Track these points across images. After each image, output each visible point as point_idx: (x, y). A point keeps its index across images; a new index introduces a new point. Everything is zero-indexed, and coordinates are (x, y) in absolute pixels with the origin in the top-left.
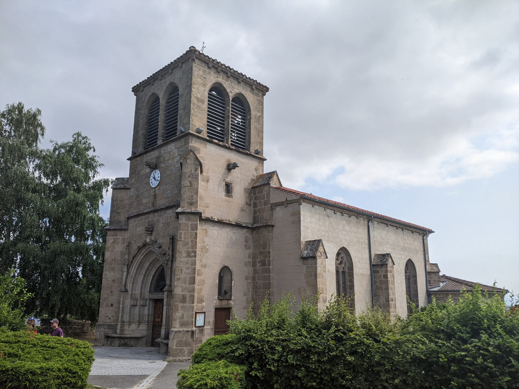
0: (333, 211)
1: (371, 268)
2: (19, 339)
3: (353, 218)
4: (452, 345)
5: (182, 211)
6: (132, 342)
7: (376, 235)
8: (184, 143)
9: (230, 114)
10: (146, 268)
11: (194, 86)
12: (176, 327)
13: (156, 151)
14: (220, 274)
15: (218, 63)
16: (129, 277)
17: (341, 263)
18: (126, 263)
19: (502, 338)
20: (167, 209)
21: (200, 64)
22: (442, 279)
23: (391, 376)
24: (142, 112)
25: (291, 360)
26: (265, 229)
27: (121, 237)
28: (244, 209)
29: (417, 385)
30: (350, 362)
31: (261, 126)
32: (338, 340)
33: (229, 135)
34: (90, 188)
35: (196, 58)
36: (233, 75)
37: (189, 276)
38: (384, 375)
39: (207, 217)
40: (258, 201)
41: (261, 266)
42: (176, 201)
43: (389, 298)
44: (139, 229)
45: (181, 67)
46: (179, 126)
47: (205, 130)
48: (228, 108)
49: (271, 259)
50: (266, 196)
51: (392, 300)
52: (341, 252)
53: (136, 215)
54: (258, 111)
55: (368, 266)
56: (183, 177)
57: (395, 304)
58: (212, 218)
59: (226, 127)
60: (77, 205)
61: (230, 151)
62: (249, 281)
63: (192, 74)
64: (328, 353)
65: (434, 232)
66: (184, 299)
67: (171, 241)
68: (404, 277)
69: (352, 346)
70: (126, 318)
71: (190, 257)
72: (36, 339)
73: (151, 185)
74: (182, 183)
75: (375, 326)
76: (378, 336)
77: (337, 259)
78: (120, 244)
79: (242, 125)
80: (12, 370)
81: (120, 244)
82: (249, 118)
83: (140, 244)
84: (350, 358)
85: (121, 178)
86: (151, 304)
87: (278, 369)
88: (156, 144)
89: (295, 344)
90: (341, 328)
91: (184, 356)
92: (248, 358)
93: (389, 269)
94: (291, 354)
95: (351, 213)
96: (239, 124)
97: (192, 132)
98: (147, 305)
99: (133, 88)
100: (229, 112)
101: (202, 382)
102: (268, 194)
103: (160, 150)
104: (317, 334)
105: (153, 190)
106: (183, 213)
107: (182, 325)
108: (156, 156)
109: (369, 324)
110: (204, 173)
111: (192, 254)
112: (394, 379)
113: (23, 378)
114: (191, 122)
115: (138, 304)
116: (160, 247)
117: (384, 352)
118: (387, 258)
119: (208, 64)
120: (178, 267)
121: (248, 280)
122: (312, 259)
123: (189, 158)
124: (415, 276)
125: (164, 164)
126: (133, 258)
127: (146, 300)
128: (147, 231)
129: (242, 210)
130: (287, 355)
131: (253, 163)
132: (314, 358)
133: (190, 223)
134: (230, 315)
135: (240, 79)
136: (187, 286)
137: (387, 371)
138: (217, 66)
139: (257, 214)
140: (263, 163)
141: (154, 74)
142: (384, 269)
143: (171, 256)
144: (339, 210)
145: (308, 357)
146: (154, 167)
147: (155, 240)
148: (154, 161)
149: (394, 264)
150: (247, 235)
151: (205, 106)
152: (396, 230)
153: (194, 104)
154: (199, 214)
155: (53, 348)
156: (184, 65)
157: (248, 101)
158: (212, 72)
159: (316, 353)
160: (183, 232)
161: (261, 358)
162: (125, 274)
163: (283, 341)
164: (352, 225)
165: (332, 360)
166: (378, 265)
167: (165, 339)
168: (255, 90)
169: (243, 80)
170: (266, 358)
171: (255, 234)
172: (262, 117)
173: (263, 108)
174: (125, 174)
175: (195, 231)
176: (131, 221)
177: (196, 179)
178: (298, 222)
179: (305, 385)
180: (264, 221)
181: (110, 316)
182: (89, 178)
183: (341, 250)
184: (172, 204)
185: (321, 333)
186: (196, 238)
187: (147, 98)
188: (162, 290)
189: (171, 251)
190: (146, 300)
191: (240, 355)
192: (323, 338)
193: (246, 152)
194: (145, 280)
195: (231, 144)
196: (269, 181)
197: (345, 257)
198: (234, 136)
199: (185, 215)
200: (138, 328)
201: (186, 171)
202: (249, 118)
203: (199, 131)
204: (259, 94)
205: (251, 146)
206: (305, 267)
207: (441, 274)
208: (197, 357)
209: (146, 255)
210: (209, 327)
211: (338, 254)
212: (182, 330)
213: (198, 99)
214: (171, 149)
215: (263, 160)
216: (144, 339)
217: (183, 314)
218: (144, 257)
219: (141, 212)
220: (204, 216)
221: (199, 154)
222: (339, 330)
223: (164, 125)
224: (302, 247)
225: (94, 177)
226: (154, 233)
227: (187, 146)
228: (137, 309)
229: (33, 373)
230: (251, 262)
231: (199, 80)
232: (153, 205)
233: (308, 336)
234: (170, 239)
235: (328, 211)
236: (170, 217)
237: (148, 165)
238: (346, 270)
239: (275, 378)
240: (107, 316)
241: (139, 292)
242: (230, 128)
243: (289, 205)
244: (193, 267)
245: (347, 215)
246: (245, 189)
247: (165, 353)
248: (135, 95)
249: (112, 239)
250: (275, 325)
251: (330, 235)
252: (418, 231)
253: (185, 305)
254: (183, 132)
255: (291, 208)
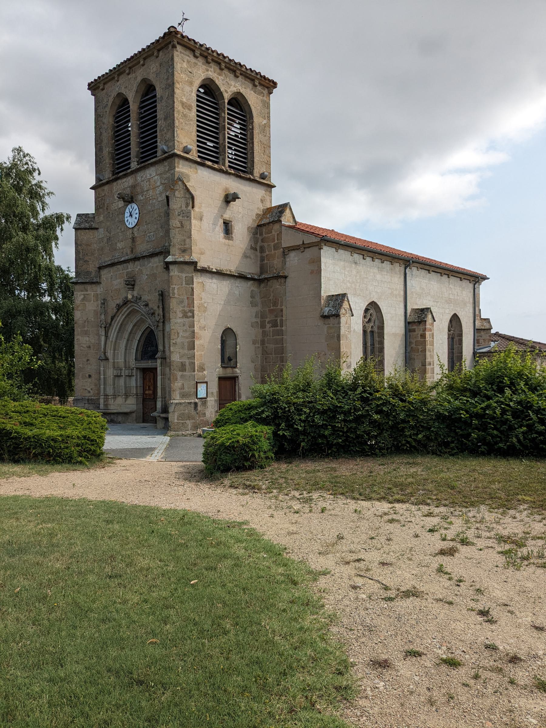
0: (362, 256)
1: (405, 326)
2: (28, 409)
3: (387, 264)
4: (476, 402)
5: (174, 260)
6: (120, 418)
7: (414, 285)
8: (168, 167)
9: (226, 124)
10: (129, 331)
11: (177, 85)
12: (176, 399)
13: (129, 178)
14: (222, 337)
15: (208, 49)
16: (109, 343)
17: (370, 320)
18: (103, 325)
19: (526, 394)
20: (151, 257)
21: (184, 52)
22: (495, 338)
23: (415, 432)
24: (105, 121)
25: (318, 420)
26: (276, 281)
27: (93, 293)
28: (248, 255)
29: (440, 440)
30: (375, 421)
31: (267, 138)
32: (365, 400)
33: (225, 153)
34: (39, 226)
35: (178, 43)
36: (228, 65)
37: (187, 340)
38: (409, 431)
39: (203, 267)
40: (265, 244)
41: (272, 327)
42: (163, 245)
43: (425, 361)
44: (115, 282)
45: (157, 57)
46: (160, 143)
47: (193, 147)
48: (223, 115)
49: (284, 319)
50: (276, 238)
51: (430, 364)
52: (369, 308)
53: (110, 264)
54: (262, 117)
55: (402, 324)
56: (171, 215)
57: (433, 368)
58: (209, 268)
59: (221, 142)
60: (28, 250)
61: (227, 176)
62: (257, 345)
63: (174, 67)
64: (353, 412)
65: (488, 279)
66: (183, 367)
67: (161, 298)
68: (446, 337)
69: (378, 406)
70: (110, 391)
71: (187, 317)
72: (44, 409)
73: (127, 224)
74: (170, 223)
75: (402, 386)
76: (405, 395)
77: (365, 317)
78: (92, 302)
79: (241, 138)
80: (33, 437)
81: (92, 302)
82: (251, 127)
83: (119, 301)
84: (376, 417)
85: (84, 214)
86: (139, 374)
87: (305, 429)
88: (129, 168)
89: (322, 405)
90: (368, 388)
91: (188, 430)
92: (274, 419)
93: (428, 326)
94: (318, 415)
95: (384, 258)
96: (237, 136)
97: (178, 153)
98: (134, 376)
99: (89, 85)
100: (224, 121)
101: (234, 440)
102: (279, 234)
103: (135, 177)
104: (344, 395)
105: (131, 231)
106: (174, 263)
107: (183, 396)
108: (130, 184)
109: (396, 384)
110: (196, 209)
111: (189, 314)
112: (417, 434)
113: (45, 445)
114: (176, 138)
115: (123, 374)
116: (147, 305)
117: (410, 410)
118: (426, 313)
119: (193, 51)
120: (173, 329)
121: (255, 344)
122: (335, 317)
123: (177, 190)
124: (461, 335)
125: (142, 196)
126: (112, 318)
127: (132, 369)
128: (128, 285)
129: (245, 256)
130: (314, 416)
131: (258, 192)
132: (341, 417)
133: (184, 275)
134: (235, 385)
135: (237, 71)
136: (186, 351)
137: (412, 427)
138: (206, 54)
139: (266, 262)
140: (271, 192)
141: (118, 66)
142: (421, 327)
143: (162, 317)
144: (370, 254)
145: (334, 417)
146: (129, 200)
147: (139, 297)
148: (128, 191)
149: (435, 321)
150: (252, 288)
151: (193, 114)
152: (440, 277)
153: (178, 111)
154: (195, 264)
155: (64, 417)
156: (161, 53)
157: (250, 103)
158: (200, 62)
159: (342, 412)
160: (176, 287)
161: (288, 419)
162: (103, 338)
163: (310, 402)
164: (385, 273)
165: (358, 420)
166: (414, 322)
167: (162, 413)
168: (258, 87)
169: (242, 72)
170: (293, 419)
171: (263, 288)
172: (268, 125)
173: (269, 113)
174: (91, 209)
175: (191, 286)
176: (104, 272)
177: (187, 217)
178: (318, 272)
179: (330, 443)
180: (275, 271)
181: (89, 389)
182: (38, 213)
183: (370, 306)
184: (158, 250)
185: (347, 394)
186: (192, 294)
187: (111, 100)
188: (153, 357)
189: (161, 309)
190: (132, 369)
191: (267, 417)
192: (349, 399)
193: (248, 176)
194: (129, 346)
195: (230, 166)
196: (280, 217)
197: (374, 314)
198: (232, 154)
199: (177, 265)
200: (125, 401)
201: (175, 207)
202: (251, 127)
203: (187, 150)
204: (264, 92)
205: (255, 168)
206: (325, 328)
207: (493, 331)
208: (219, 422)
209: (128, 314)
210: (212, 399)
211: (366, 310)
212: (183, 401)
213: (183, 104)
214: (151, 175)
215: (271, 186)
216: (134, 415)
217: (183, 384)
218: (125, 317)
219: (116, 261)
220: (200, 265)
221: (188, 182)
222: (365, 391)
223: (138, 140)
224: (322, 303)
225: (43, 210)
226: (136, 287)
227: (172, 171)
228: (122, 381)
229: (55, 440)
230: (259, 322)
231: (183, 76)
232: (132, 251)
233: (334, 397)
234: (159, 295)
235: (356, 256)
236: (157, 267)
237: (122, 197)
238: (376, 329)
239: (302, 437)
240: (86, 389)
241: (123, 360)
242: (227, 144)
243: (307, 250)
244: (192, 329)
245: (380, 261)
246: (248, 228)
247: (164, 428)
248: (92, 94)
249: (81, 294)
250: (300, 388)
251: (357, 287)
252: (469, 278)
253: (185, 373)
254: (167, 152)
255: (309, 253)
